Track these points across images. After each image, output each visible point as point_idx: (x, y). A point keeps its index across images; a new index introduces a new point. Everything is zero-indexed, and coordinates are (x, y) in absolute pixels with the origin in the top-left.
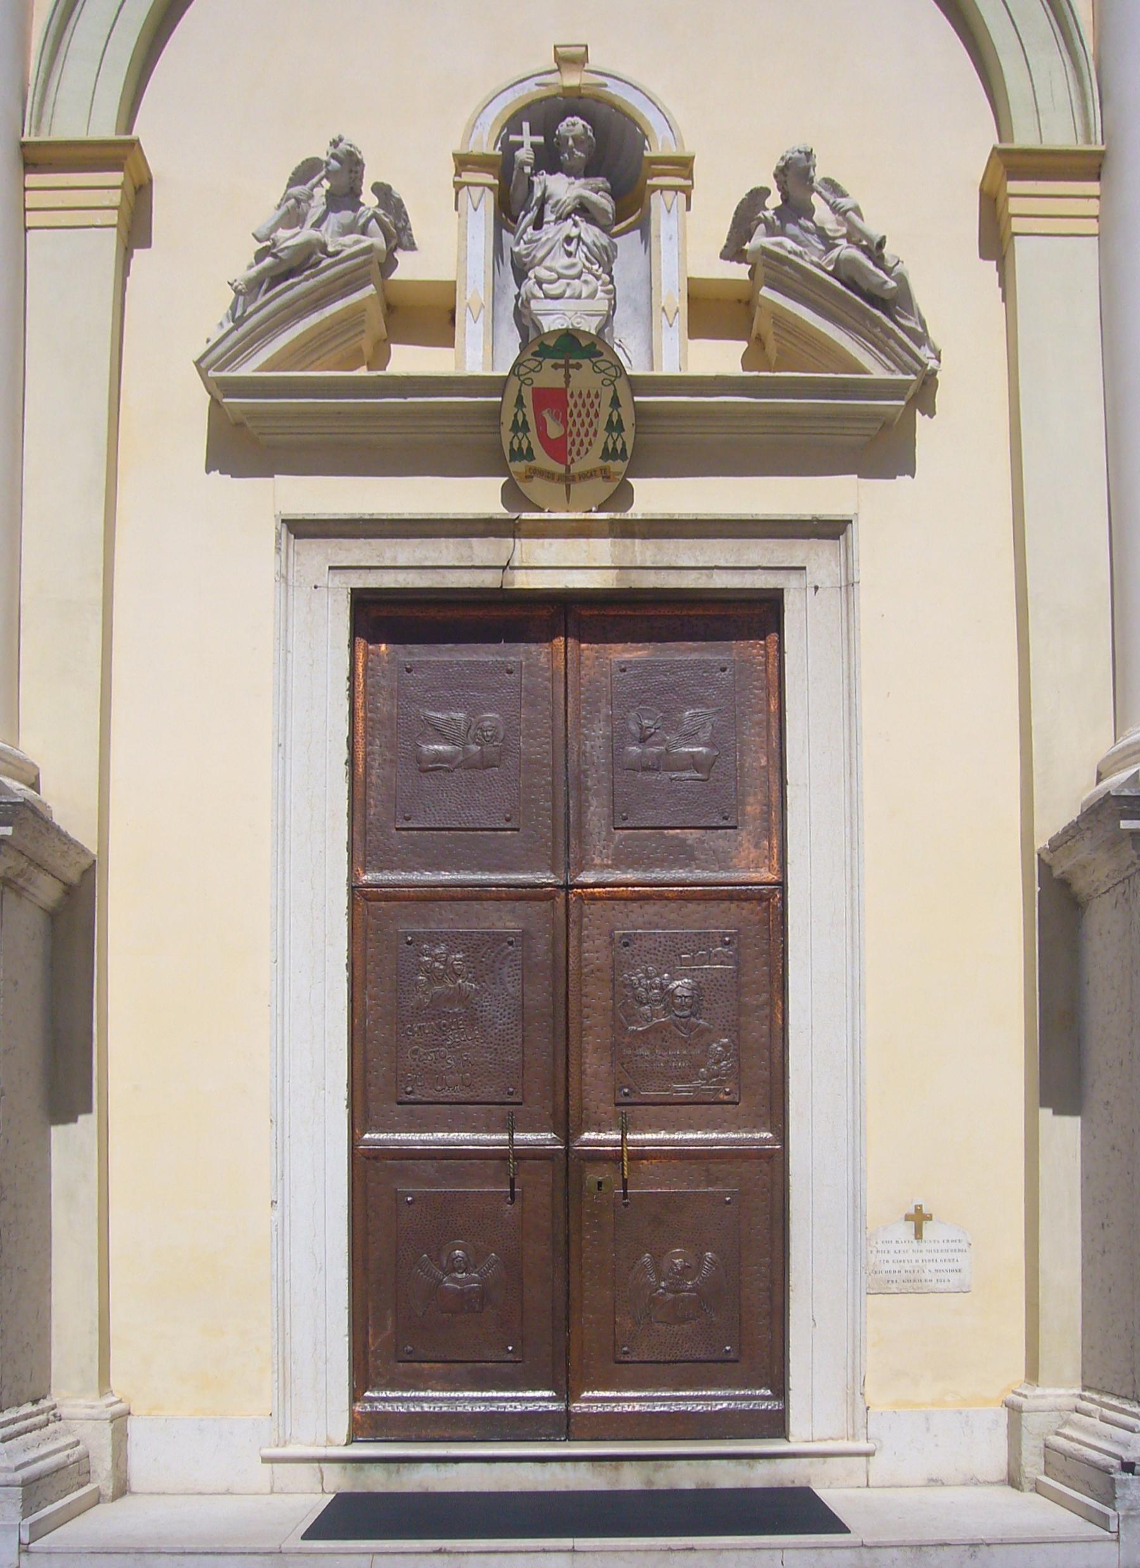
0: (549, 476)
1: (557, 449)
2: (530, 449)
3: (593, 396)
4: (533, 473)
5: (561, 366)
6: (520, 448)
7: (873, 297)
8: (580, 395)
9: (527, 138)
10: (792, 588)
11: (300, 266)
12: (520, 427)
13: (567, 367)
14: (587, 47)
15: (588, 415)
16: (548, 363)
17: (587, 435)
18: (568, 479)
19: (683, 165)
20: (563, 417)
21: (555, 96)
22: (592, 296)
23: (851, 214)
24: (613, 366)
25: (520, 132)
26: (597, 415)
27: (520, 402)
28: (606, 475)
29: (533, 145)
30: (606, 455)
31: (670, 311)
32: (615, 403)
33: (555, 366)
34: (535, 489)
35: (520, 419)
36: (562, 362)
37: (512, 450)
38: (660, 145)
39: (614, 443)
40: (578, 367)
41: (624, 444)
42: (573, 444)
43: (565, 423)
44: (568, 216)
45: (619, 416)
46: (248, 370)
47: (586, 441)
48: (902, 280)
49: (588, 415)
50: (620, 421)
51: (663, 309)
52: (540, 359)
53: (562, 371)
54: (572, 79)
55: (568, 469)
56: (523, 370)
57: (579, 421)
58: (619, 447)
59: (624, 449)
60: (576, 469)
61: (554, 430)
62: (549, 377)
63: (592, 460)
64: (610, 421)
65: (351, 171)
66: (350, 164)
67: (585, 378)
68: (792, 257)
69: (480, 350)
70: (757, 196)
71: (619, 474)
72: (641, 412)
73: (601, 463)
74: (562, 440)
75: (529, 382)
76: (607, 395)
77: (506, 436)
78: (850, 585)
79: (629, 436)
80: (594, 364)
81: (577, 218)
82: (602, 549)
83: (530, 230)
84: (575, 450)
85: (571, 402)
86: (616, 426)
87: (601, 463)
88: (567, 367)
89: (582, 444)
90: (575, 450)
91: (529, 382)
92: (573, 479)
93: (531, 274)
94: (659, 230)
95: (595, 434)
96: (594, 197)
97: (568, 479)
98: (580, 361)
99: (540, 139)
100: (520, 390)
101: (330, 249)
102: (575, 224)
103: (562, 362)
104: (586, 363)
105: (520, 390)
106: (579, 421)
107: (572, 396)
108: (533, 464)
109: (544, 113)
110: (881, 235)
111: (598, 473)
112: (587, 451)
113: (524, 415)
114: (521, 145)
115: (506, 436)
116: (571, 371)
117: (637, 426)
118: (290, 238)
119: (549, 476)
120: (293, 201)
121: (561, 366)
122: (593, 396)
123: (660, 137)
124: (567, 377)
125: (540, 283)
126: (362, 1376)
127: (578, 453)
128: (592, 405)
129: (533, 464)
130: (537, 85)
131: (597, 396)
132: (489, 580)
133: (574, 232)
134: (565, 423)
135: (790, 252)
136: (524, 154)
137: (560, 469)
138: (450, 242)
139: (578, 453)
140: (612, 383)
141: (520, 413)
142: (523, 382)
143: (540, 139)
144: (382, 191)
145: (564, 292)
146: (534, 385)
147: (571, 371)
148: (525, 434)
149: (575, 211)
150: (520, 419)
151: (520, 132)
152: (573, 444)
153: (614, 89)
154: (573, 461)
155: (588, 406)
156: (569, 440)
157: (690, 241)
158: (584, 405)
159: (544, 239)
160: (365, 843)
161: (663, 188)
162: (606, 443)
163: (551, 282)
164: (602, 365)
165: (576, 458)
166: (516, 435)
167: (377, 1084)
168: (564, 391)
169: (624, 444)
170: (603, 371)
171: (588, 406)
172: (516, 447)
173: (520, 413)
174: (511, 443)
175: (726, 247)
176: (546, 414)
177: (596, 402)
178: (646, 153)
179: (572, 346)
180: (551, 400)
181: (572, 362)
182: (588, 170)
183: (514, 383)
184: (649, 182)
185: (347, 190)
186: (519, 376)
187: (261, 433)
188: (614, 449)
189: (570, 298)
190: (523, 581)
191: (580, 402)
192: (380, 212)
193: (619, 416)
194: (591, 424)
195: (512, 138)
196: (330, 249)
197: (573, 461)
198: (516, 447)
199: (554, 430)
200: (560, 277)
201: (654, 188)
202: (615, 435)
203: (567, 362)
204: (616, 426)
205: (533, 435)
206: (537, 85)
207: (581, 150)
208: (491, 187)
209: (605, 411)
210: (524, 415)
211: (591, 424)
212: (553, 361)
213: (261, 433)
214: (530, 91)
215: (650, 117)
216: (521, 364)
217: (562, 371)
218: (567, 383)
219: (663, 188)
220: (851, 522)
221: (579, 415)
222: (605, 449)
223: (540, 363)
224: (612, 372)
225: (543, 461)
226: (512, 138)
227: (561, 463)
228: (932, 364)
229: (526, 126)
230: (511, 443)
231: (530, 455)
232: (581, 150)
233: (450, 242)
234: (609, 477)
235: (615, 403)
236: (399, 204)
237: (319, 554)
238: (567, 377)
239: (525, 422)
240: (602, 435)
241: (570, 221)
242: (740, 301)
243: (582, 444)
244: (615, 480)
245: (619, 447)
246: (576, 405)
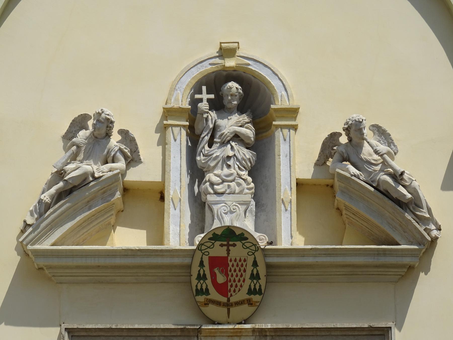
0: (218, 303)
1: (222, 289)
2: (207, 290)
3: (242, 261)
4: (208, 302)
5: (225, 245)
6: (202, 289)
8: (235, 260)
9: (205, 96)
11: (79, 185)
12: (201, 277)
13: (228, 245)
14: (238, 43)
15: (240, 270)
16: (218, 243)
17: (239, 281)
18: (228, 305)
19: (293, 112)
21: (220, 70)
22: (241, 192)
23: (385, 156)
24: (254, 245)
25: (200, 92)
26: (245, 271)
27: (202, 264)
28: (250, 302)
29: (209, 100)
30: (250, 292)
31: (286, 201)
32: (255, 264)
33: (222, 245)
34: (212, 311)
35: (202, 273)
36: (225, 243)
37: (197, 290)
38: (281, 101)
39: (255, 285)
40: (234, 245)
41: (260, 286)
42: (231, 286)
43: (227, 275)
44: (228, 142)
45: (257, 271)
47: (239, 284)
48: (414, 192)
49: (240, 270)
50: (258, 274)
51: (283, 200)
52: (213, 242)
53: (225, 248)
54: (230, 63)
55: (229, 300)
56: (203, 247)
57: (235, 274)
58: (257, 287)
59: (260, 289)
60: (232, 300)
61: (221, 279)
62: (218, 251)
63: (242, 295)
64: (252, 274)
65: (107, 127)
66: (105, 126)
67: (238, 251)
68: (353, 178)
69: (178, 233)
71: (257, 302)
72: (269, 266)
73: (248, 297)
74: (226, 284)
75: (207, 253)
76: (250, 260)
77: (194, 282)
79: (263, 281)
80: (243, 244)
81: (233, 144)
83: (207, 147)
84: (232, 289)
85: (230, 264)
86: (255, 277)
87: (248, 297)
88: (228, 245)
89: (236, 286)
90: (232, 289)
91: (207, 253)
92: (232, 305)
93: (207, 178)
94: (280, 152)
95: (244, 281)
96: (243, 130)
97: (228, 305)
98: (235, 243)
99: (212, 96)
100: (202, 258)
101: (96, 175)
102: (232, 148)
103: (225, 243)
104: (239, 244)
105: (202, 258)
106: (235, 274)
107: (231, 261)
108: (209, 297)
109: (214, 82)
110: (402, 170)
111: (246, 302)
112: (239, 290)
113: (204, 271)
114: (201, 100)
115: (194, 282)
116: (230, 248)
117: (267, 276)
119: (218, 303)
120: (75, 148)
121: (225, 245)
122: (242, 261)
123: (279, 95)
124: (228, 251)
125: (212, 184)
127: (234, 291)
128: (242, 265)
129: (209, 297)
130: (210, 64)
131: (245, 260)
133: (231, 153)
134: (227, 275)
135: (352, 175)
136: (204, 106)
137: (224, 300)
138: (161, 162)
139: (234, 291)
140: (253, 254)
141: (202, 270)
142: (203, 254)
143: (212, 96)
144: (124, 133)
145: (226, 190)
146: (210, 255)
147: (230, 248)
148: (204, 281)
149: (232, 139)
150: (202, 273)
151: (200, 92)
152: (231, 286)
153: (254, 67)
154: (231, 295)
155: (240, 266)
156: (229, 284)
157: (297, 157)
158: (237, 266)
159: (214, 155)
161: (282, 127)
162: (250, 286)
163: (218, 184)
164: (248, 245)
165: (233, 294)
166: (199, 281)
168: (226, 258)
169: (260, 286)
170: (247, 248)
171: (240, 266)
172: (199, 288)
173: (202, 270)
174: (197, 286)
175: (318, 160)
176: (216, 270)
177: (244, 264)
178: (272, 106)
179: (230, 235)
180: (219, 263)
181: (231, 243)
183: (198, 255)
184: (274, 123)
185: (105, 135)
186: (201, 250)
187: (54, 276)
188: (255, 289)
189: (229, 194)
191: (235, 264)
192: (123, 147)
193: (257, 271)
194: (241, 276)
195: (197, 96)
196: (96, 175)
197: (231, 295)
198: (199, 288)
199: (221, 279)
200: (223, 181)
201: (277, 127)
202: (255, 281)
203: (228, 243)
204: (255, 277)
205: (209, 281)
206: (210, 64)
207: (236, 97)
208: (184, 126)
209: (249, 268)
210: (204, 271)
211: (241, 276)
212: (220, 243)
213: (54, 276)
214: (207, 68)
216: (203, 244)
217: (225, 248)
218: (228, 253)
219: (282, 127)
220: (391, 328)
221: (235, 271)
222: (250, 289)
223: (213, 244)
224: (253, 248)
225: (214, 295)
226: (197, 96)
227: (224, 296)
228: (435, 233)
229: (204, 88)
230: (197, 286)
231: (207, 292)
232: (236, 97)
233: (161, 162)
234: (252, 304)
235: (255, 264)
236: (133, 140)
238: (228, 251)
239: (204, 275)
240: (248, 281)
241: (229, 146)
242: (328, 185)
243: (236, 286)
244: (255, 305)
245: (257, 287)
246: (233, 266)
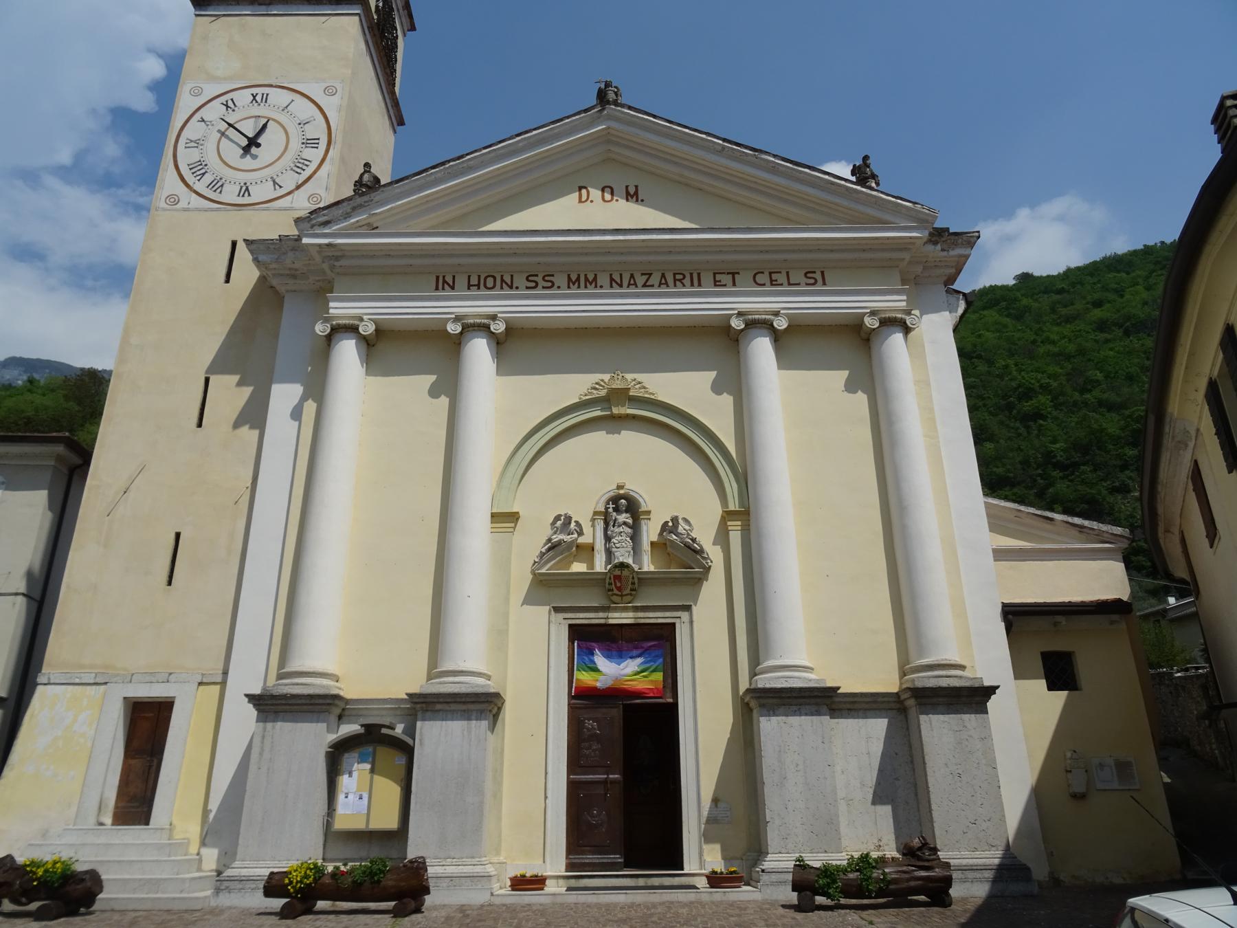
1: (619, 589)
7: (694, 551)
10: (677, 621)
12: (610, 584)
19: (649, 512)
20: (620, 582)
34: (615, 598)
38: (643, 508)
46: (543, 571)
54: (622, 492)
62: (617, 572)
63: (628, 591)
66: (568, 519)
67: (626, 572)
69: (600, 565)
70: (666, 523)
78: (691, 622)
82: (631, 614)
86: (633, 583)
109: (615, 500)
118: (556, 538)
126: (570, 851)
132: (602, 621)
138: (592, 534)
144: (577, 522)
157: (650, 532)
160: (964, 379)
167: (575, 761)
180: (617, 578)
182: (626, 512)
190: (611, 621)
207: (624, 506)
214: (612, 494)
215: (643, 503)
225: (616, 591)
237: (561, 616)
